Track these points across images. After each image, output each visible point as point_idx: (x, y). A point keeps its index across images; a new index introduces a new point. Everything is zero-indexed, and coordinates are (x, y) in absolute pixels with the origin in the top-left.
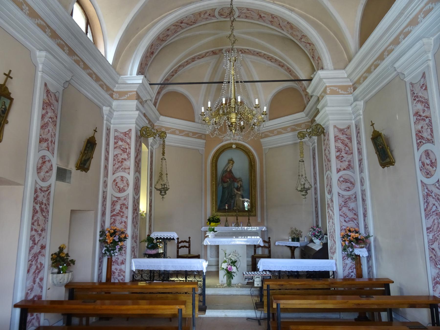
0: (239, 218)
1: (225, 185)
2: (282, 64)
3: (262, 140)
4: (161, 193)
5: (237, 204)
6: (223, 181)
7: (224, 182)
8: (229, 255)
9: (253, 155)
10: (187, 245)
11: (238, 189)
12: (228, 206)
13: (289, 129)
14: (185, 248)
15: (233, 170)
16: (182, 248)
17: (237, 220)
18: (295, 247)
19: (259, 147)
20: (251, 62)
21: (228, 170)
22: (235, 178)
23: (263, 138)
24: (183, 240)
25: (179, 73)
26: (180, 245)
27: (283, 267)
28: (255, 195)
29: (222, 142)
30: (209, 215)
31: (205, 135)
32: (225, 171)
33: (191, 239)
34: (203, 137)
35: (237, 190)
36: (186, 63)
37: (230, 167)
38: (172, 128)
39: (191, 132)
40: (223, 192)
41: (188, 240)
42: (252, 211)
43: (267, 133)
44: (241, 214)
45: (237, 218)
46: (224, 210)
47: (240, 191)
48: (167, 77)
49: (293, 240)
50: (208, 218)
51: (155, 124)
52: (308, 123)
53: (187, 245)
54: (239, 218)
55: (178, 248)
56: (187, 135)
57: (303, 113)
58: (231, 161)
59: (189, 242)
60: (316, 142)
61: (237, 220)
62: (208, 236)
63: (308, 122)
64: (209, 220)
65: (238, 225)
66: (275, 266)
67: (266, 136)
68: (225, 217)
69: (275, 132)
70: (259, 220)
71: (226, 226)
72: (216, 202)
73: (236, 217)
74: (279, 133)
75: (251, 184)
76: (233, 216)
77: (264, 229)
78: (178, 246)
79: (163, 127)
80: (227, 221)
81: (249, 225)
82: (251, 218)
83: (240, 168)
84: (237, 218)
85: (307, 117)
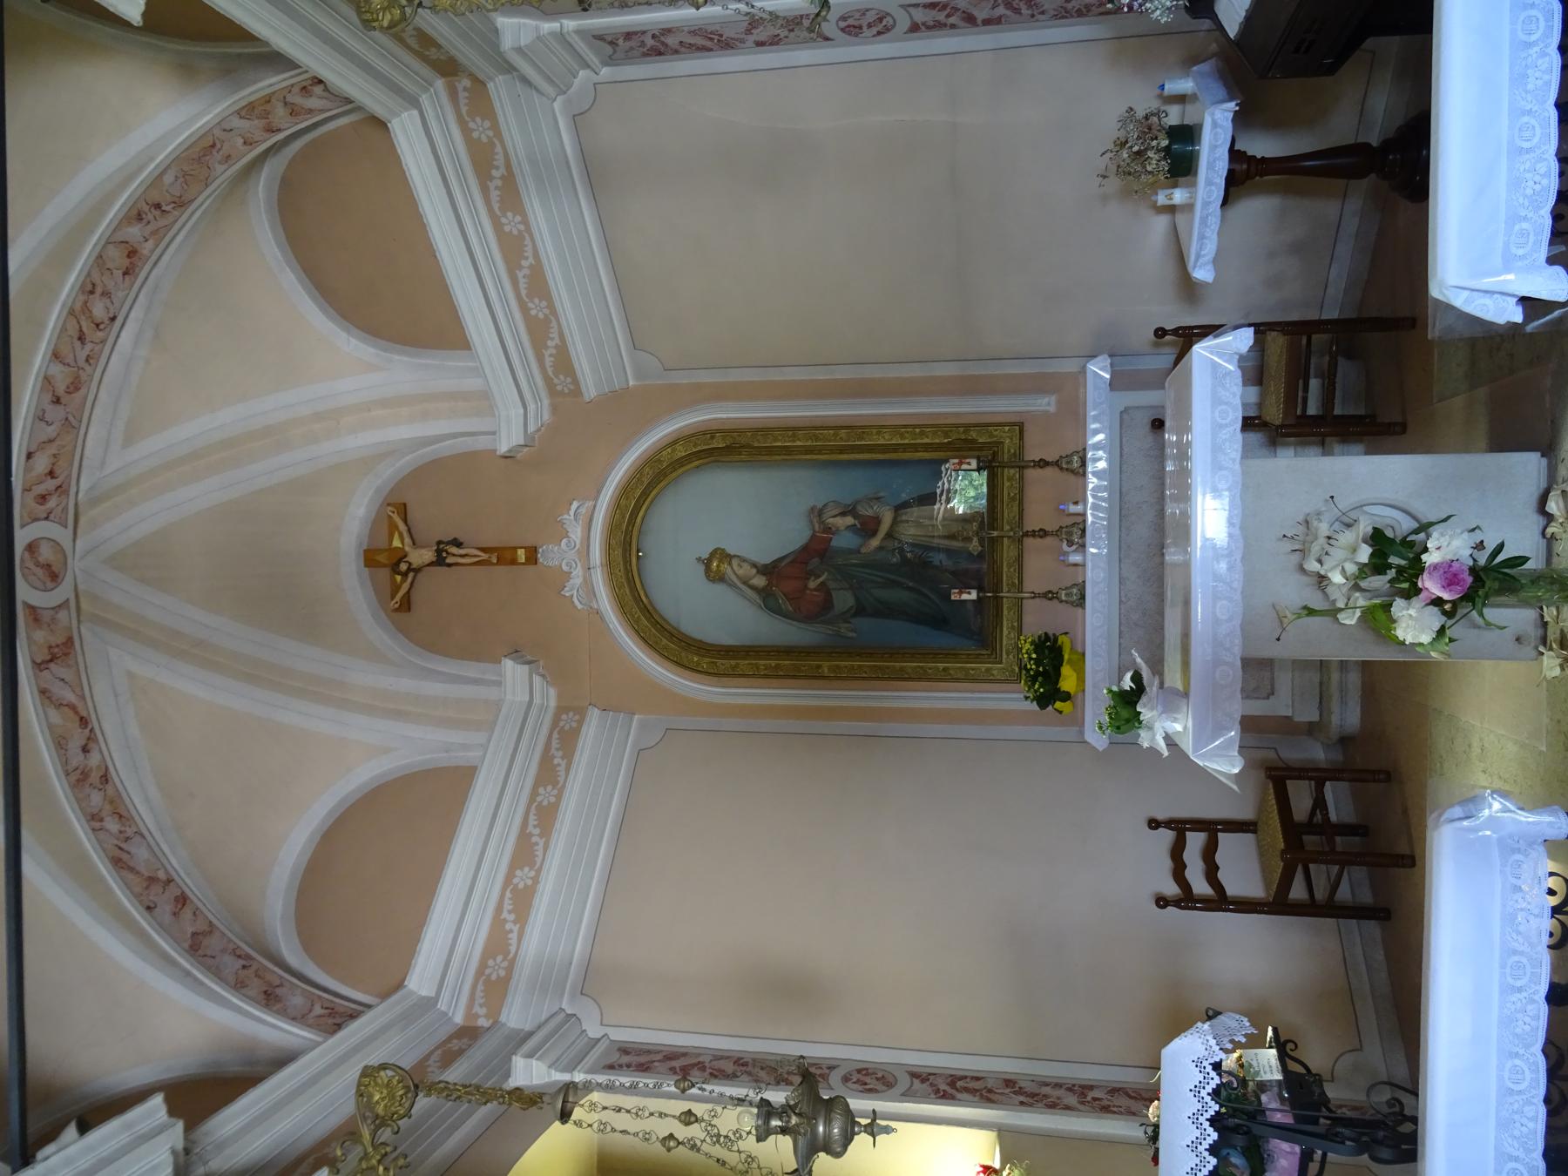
0: (1031, 524)
1: (844, 600)
2: (116, 257)
3: (590, 390)
4: (828, 1150)
5: (952, 537)
6: (821, 611)
7: (828, 604)
8: (1322, 579)
9: (675, 442)
10: (1195, 841)
11: (868, 528)
12: (966, 587)
13: (511, 223)
14: (1219, 858)
15: (766, 559)
16: (1221, 876)
17: (1043, 533)
18: (1235, 155)
19: (631, 409)
20: (129, 440)
21: (760, 581)
22: (805, 549)
23: (576, 382)
24: (1168, 864)
25: (177, 862)
26: (1201, 887)
27: (1518, 80)
28: (896, 429)
29: (602, 618)
30: (1016, 699)
31: (561, 710)
32: (767, 599)
33: (1161, 816)
34: (568, 720)
35: (874, 533)
36: (112, 825)
37: (746, 570)
38: (499, 909)
39: (534, 793)
40: (885, 611)
41: (1167, 836)
42: (996, 452)
43: (548, 361)
44: (1008, 513)
45: (1033, 534)
46: (989, 607)
47: (877, 521)
48: (176, 940)
49: (1182, 166)
50: (1035, 706)
51: (459, 1019)
52: (462, 95)
53: (1195, 841)
54: (1031, 524)
55: (1220, 901)
56: (546, 816)
57: (395, 125)
58: (715, 565)
59: (1181, 827)
60: (555, 26)
61: (1043, 533)
62: (1170, 741)
63: (453, 94)
64: (1044, 701)
65: (1075, 532)
66: (1517, 152)
67: (564, 363)
68: (1029, 605)
69: (537, 309)
70: (1045, 404)
71: (1081, 601)
72: (935, 655)
73: (1028, 541)
74: (538, 285)
75: (832, 450)
76: (1020, 560)
77: (1100, 370)
78: (1209, 905)
79: (483, 966)
80: (1050, 596)
81: (1074, 464)
82: (1032, 454)
83: (753, 516)
84: (1033, 534)
85: (424, 100)
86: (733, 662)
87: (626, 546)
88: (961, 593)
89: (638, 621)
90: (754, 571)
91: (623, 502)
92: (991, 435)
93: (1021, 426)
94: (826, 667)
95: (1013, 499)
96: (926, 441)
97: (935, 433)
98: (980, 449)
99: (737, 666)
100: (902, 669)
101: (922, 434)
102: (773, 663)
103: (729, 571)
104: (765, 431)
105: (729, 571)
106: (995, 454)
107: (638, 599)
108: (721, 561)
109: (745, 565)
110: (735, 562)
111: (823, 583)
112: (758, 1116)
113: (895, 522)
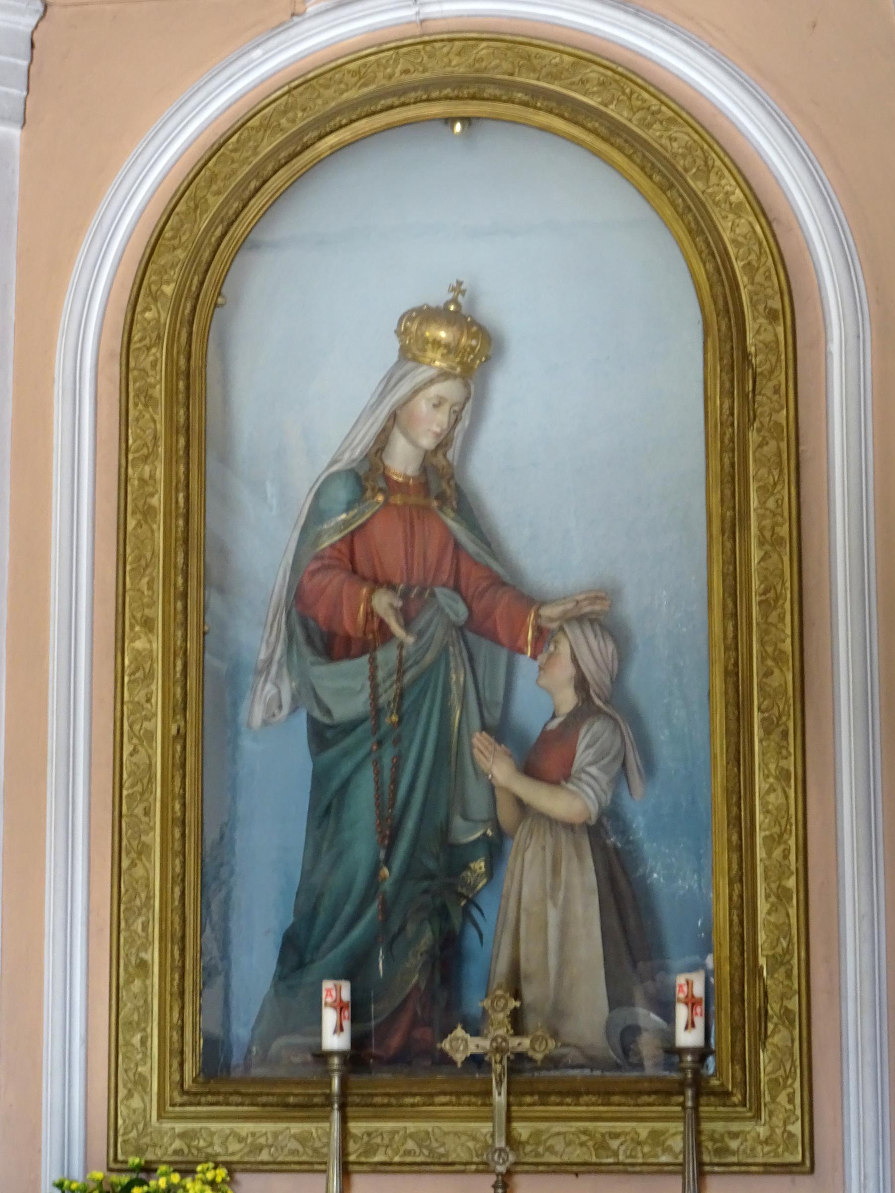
9: (761, 211)
21: (402, 460)
35: (529, 769)
53: (679, 1168)
58: (460, 341)
86: (159, 392)
87: (470, 87)
88: (340, 1007)
89: (267, 126)
90: (427, 442)
91: (593, 73)
92: (776, 1085)
93: (807, 1166)
94: (148, 644)
95: (601, 1146)
96: (762, 906)
97: (782, 930)
98: (738, 1058)
99: (149, 401)
100: (144, 850)
101: (781, 896)
102: (158, 501)
103: (424, 373)
104: (795, 463)
105: (424, 373)
106: (724, 1095)
107: (325, 126)
108: (450, 349)
109: (442, 418)
110: (449, 389)
111: (384, 634)
112: (406, 477)
113: (552, 823)
